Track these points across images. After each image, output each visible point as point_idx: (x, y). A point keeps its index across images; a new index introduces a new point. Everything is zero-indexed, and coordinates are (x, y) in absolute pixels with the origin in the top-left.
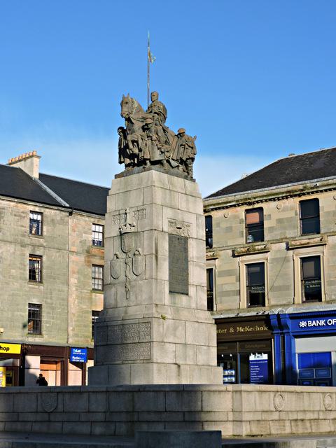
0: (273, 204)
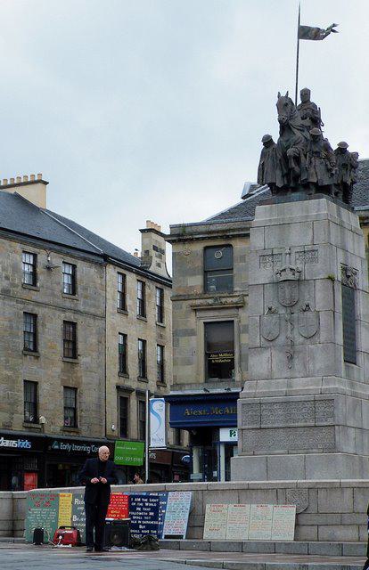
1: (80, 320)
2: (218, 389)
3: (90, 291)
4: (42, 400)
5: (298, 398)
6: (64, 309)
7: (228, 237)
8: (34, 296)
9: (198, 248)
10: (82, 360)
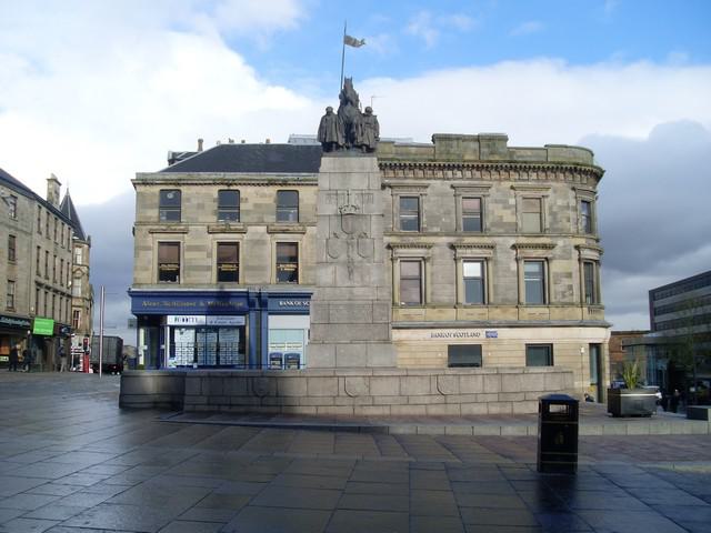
0: (250, 189)
1: (18, 235)
3: (25, 216)
6: (10, 227)
9: (157, 189)
10: (19, 262)
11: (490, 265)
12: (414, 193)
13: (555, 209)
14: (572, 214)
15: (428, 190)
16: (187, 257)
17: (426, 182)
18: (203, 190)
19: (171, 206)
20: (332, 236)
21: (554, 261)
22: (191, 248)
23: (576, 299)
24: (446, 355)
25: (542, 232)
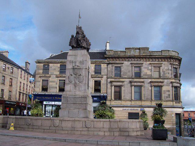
1: (13, 79)
2: (60, 94)
4: (4, 93)
5: (77, 96)
7: (49, 63)
8: (5, 73)
9: (42, 65)
10: (13, 86)
11: (143, 88)
12: (119, 65)
13: (164, 70)
14: (170, 72)
15: (123, 65)
16: (50, 84)
17: (123, 62)
18: (55, 65)
19: (46, 69)
20: (70, 75)
21: (164, 87)
22: (51, 82)
23: (171, 99)
24: (128, 116)
25: (160, 77)
